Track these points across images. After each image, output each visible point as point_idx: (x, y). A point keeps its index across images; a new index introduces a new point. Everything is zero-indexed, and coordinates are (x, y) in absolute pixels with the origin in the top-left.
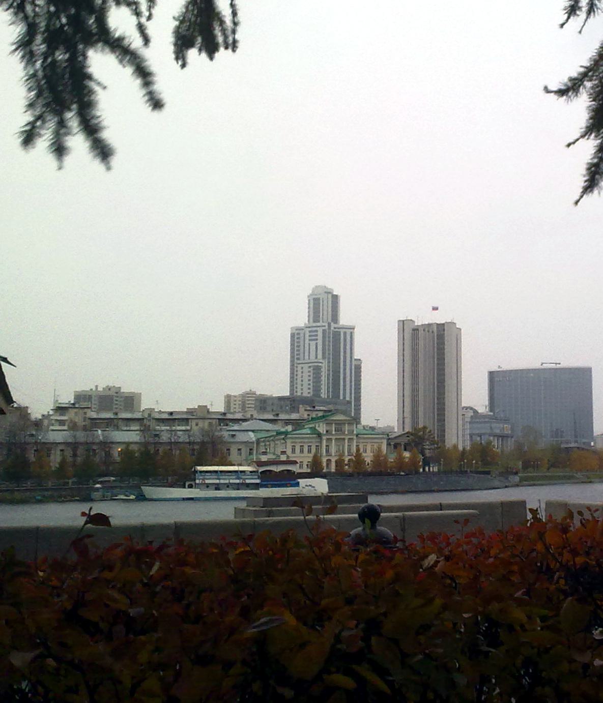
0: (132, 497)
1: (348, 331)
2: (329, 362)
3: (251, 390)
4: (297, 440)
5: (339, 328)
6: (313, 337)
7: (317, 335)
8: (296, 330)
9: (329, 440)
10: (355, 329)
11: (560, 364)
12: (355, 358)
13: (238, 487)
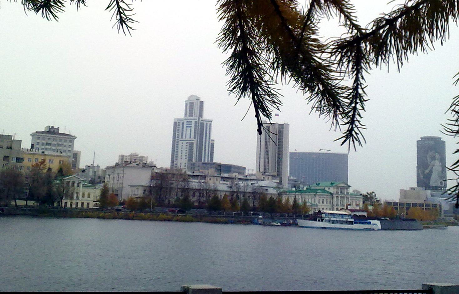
0: (279, 224)
1: (209, 123)
2: (197, 141)
3: (135, 153)
4: (325, 196)
5: (203, 121)
6: (189, 125)
7: (187, 124)
8: (178, 120)
9: (337, 197)
10: (212, 122)
11: (330, 150)
12: (212, 139)
13: (342, 222)
